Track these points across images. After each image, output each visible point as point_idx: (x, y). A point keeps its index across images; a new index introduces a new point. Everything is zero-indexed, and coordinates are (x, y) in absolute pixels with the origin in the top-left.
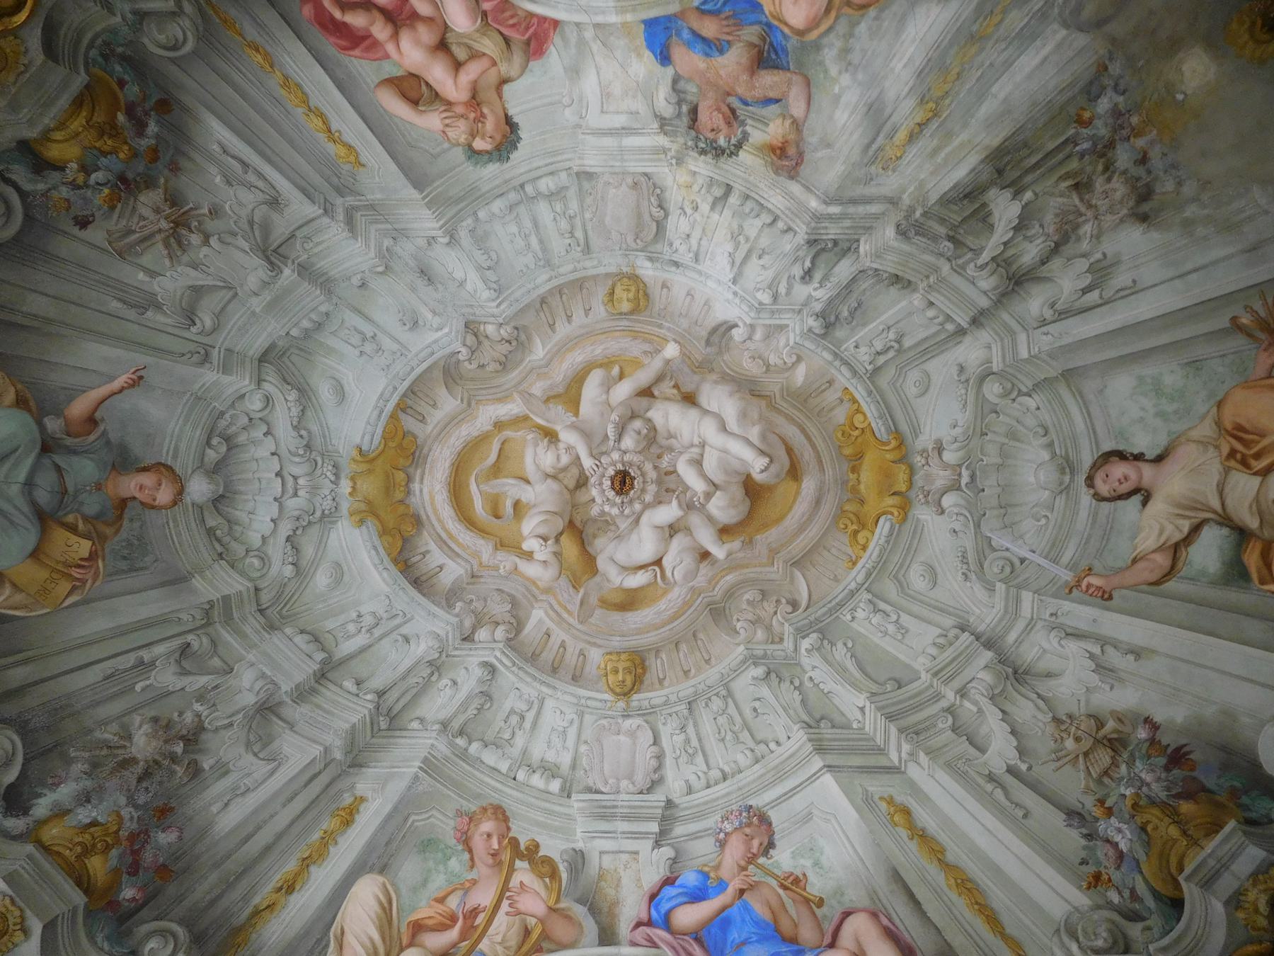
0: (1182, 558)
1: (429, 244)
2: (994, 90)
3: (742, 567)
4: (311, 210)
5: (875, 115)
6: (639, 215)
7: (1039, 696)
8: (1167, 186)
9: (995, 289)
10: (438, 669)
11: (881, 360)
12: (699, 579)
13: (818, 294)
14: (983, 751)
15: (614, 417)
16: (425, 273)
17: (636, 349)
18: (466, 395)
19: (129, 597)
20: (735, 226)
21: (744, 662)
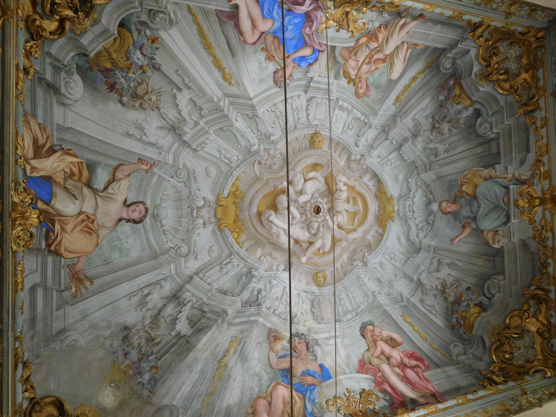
0: (111, 175)
2: (197, 375)
3: (276, 178)
5: (243, 358)
6: (320, 308)
7: (165, 119)
9: (184, 292)
11: (228, 260)
13: (255, 285)
14: (191, 99)
15: (320, 234)
16: (380, 282)
17: (316, 259)
21: (278, 142)
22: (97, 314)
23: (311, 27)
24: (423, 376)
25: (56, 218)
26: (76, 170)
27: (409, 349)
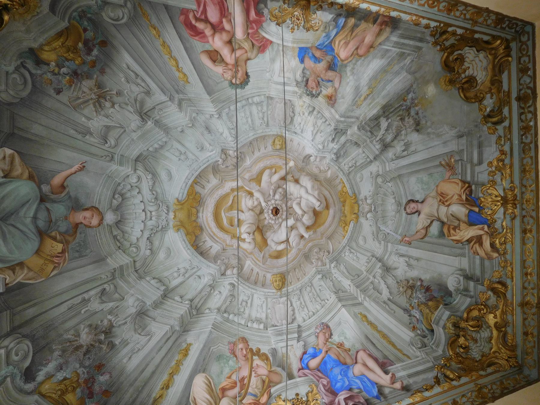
1: (211, 117)
4: (164, 98)
5: (357, 89)
8: (423, 122)
10: (213, 288)
11: (351, 169)
12: (301, 245)
14: (381, 294)
15: (273, 187)
18: (221, 178)
19: (79, 270)
20: (315, 121)
21: (315, 273)
22: (438, 143)
23: (324, 386)
24: (199, 6)
25: (465, 202)
26: (452, 231)
27: (198, 45)
